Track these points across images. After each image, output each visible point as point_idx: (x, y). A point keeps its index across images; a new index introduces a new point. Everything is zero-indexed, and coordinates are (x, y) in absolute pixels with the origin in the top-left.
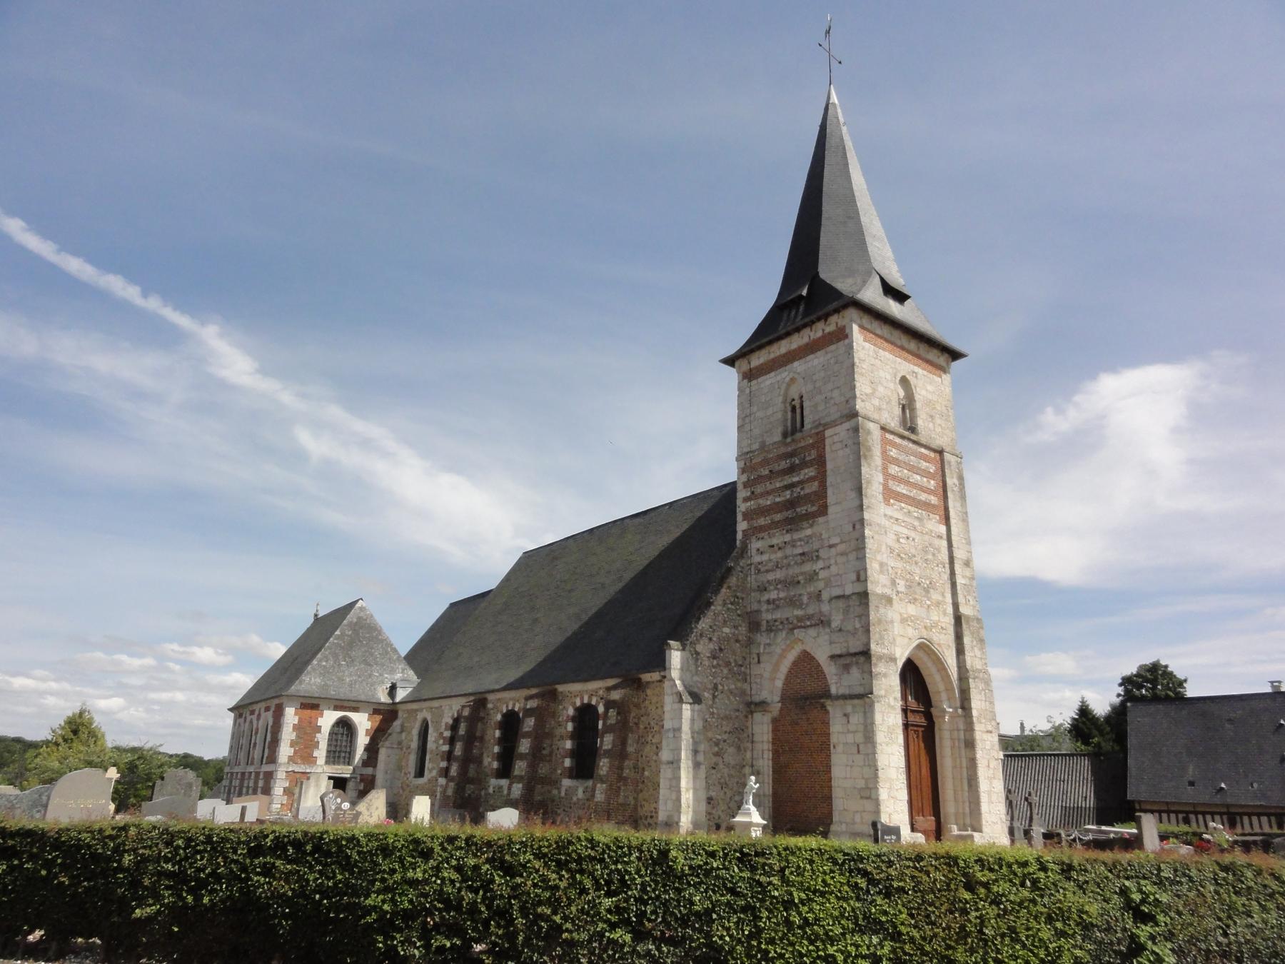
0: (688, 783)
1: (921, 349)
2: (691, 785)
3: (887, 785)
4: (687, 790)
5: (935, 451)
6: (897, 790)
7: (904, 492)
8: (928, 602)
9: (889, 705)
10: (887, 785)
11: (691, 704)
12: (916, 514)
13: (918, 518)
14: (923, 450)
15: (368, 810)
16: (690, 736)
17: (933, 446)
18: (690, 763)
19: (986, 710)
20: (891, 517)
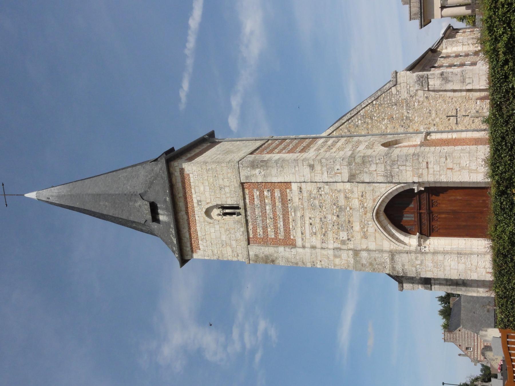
0: (474, 291)
1: (179, 196)
2: (475, 289)
3: (469, 272)
4: (478, 292)
5: (243, 189)
6: (471, 265)
7: (282, 223)
8: (348, 209)
9: (421, 264)
10: (469, 272)
11: (431, 286)
12: (293, 214)
13: (295, 212)
14: (247, 201)
15: (494, 360)
16: (449, 287)
17: (241, 194)
18: (463, 289)
19: (412, 166)
20: (303, 239)
